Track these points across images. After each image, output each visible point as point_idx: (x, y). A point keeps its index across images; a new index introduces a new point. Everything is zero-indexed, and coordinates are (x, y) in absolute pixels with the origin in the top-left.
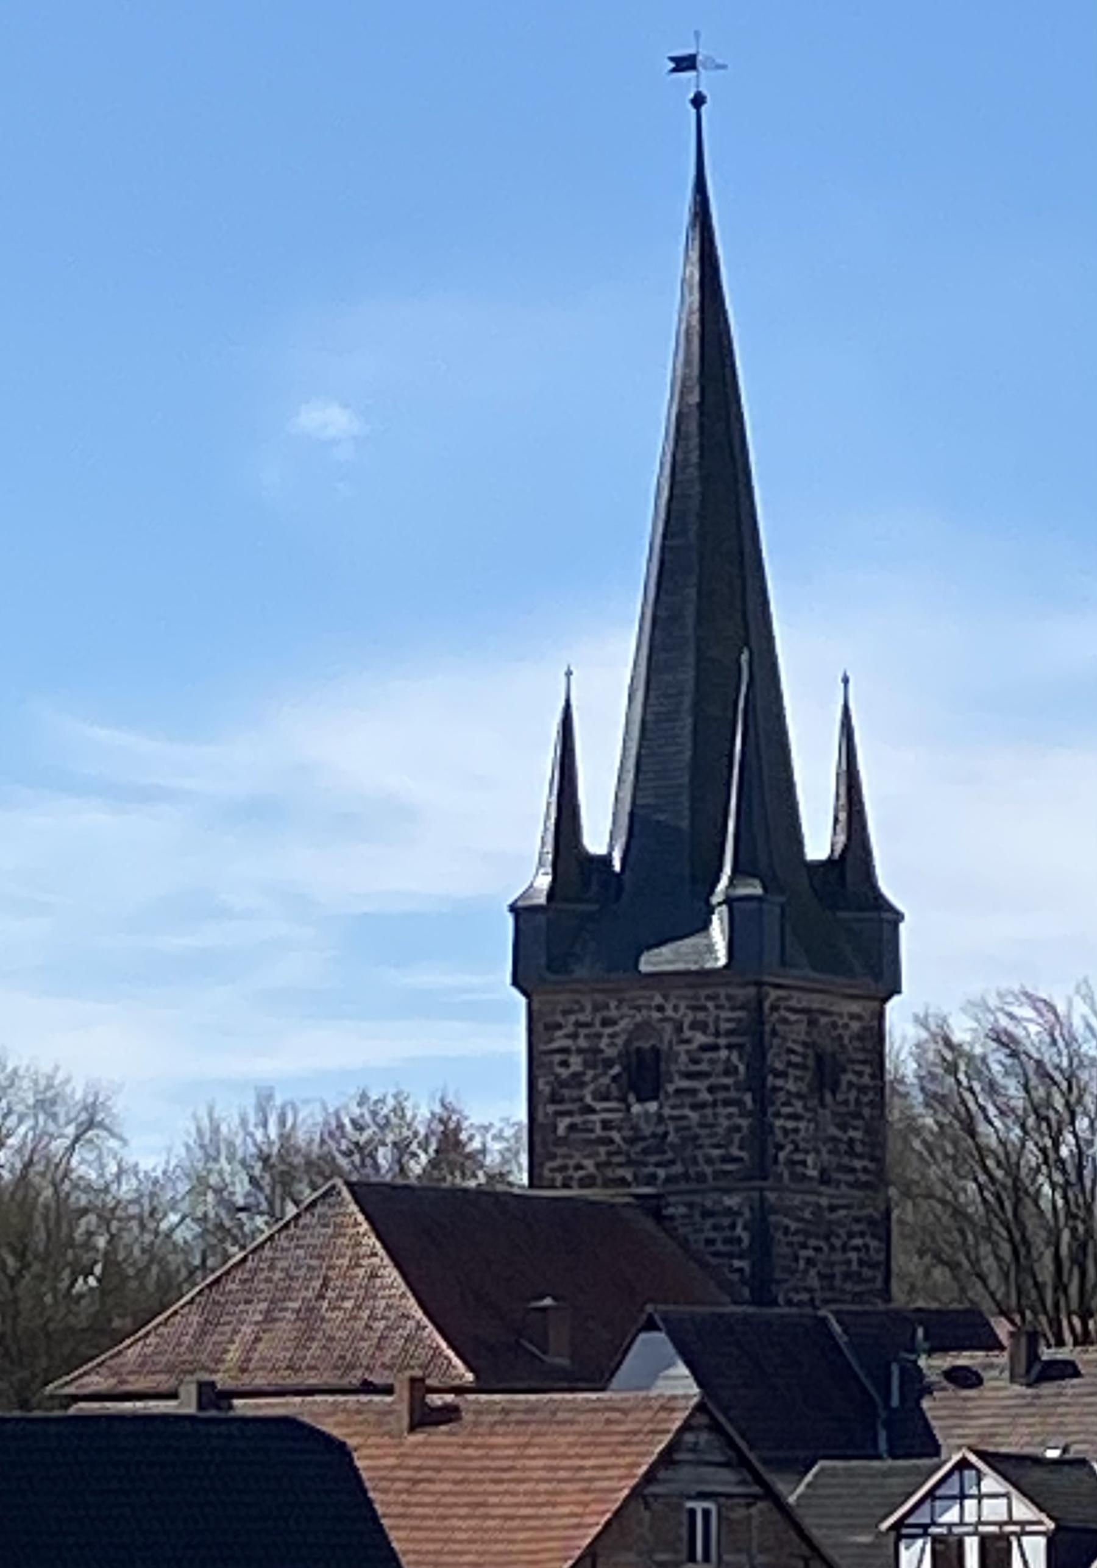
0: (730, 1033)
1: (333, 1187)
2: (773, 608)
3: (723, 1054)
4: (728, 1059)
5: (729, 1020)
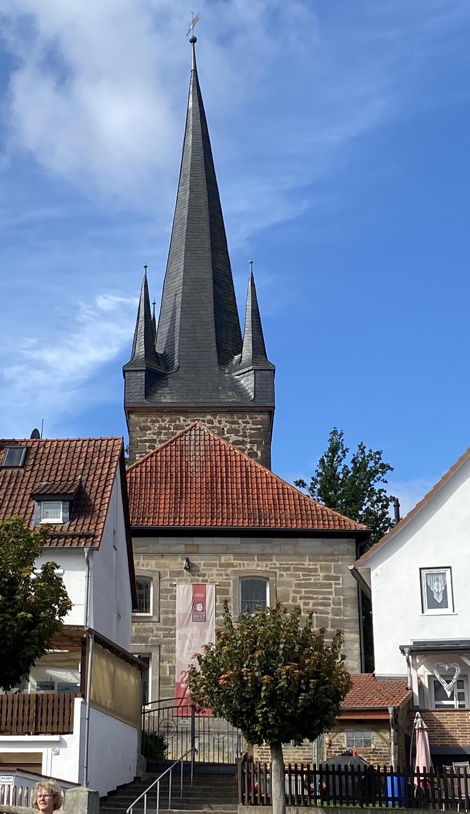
0: (251, 436)
1: (164, 637)
2: (219, 189)
3: (248, 446)
4: (251, 449)
5: (251, 429)
